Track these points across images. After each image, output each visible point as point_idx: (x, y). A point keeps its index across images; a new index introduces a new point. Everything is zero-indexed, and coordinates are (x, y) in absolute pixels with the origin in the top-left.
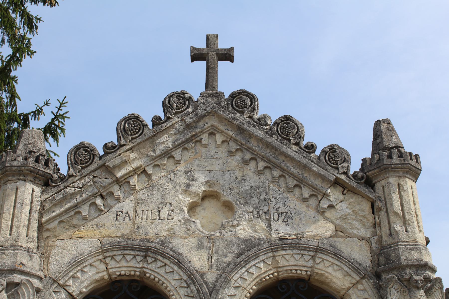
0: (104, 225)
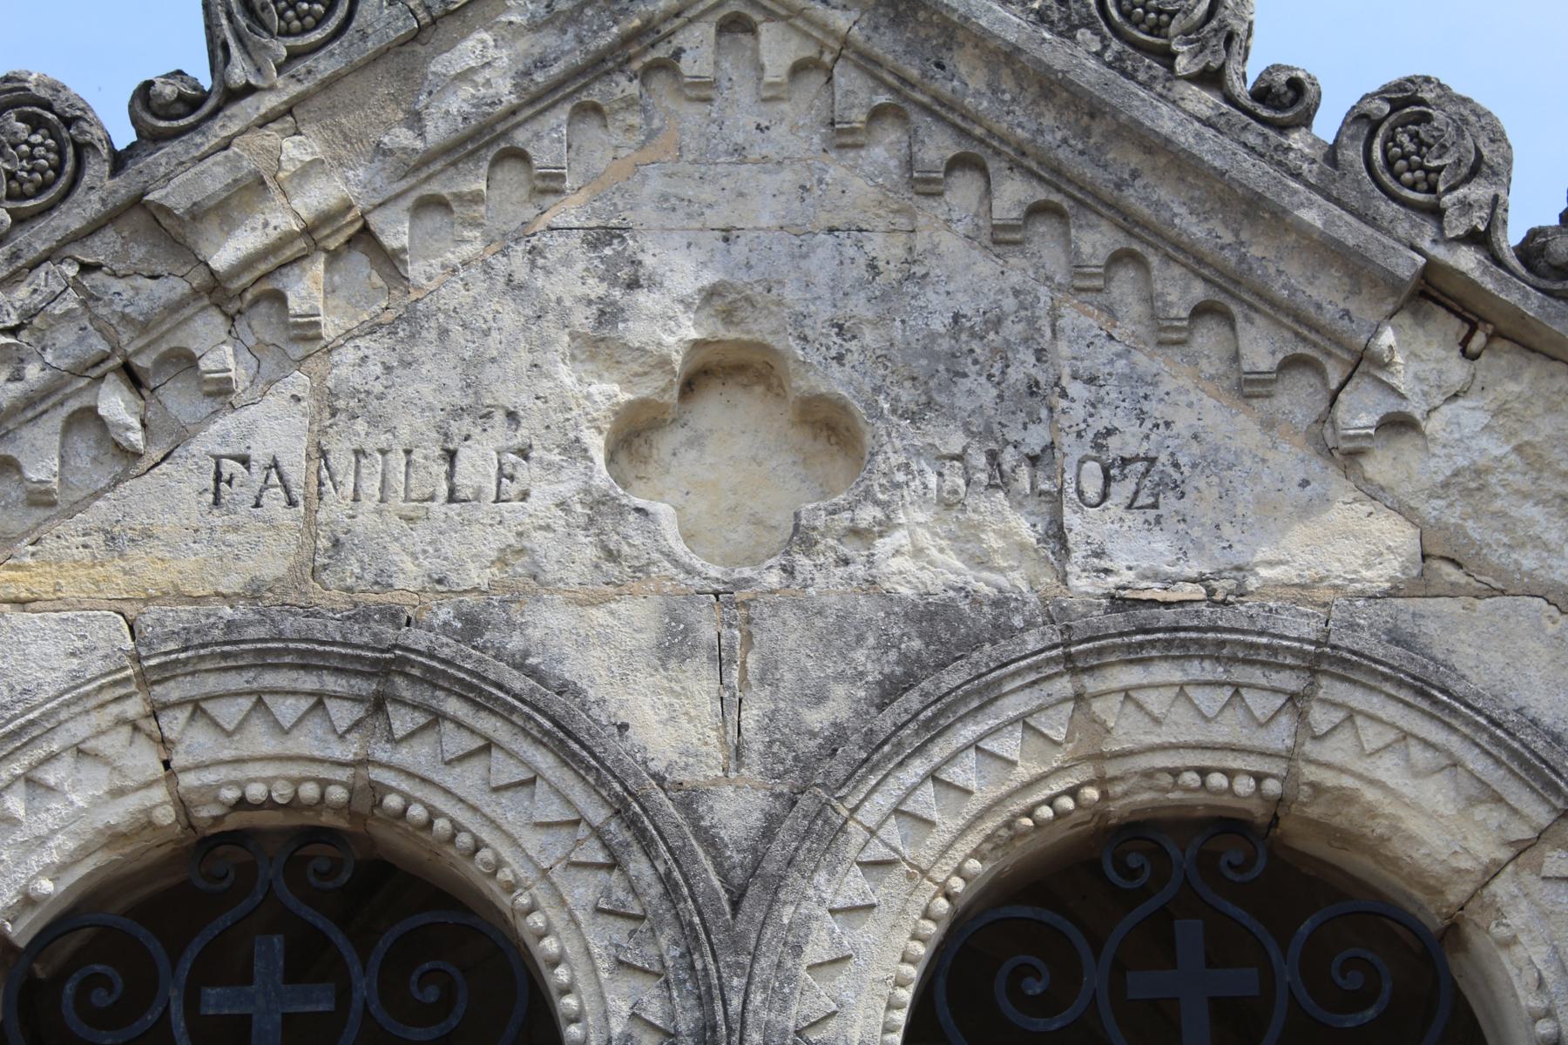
0: (147, 534)
